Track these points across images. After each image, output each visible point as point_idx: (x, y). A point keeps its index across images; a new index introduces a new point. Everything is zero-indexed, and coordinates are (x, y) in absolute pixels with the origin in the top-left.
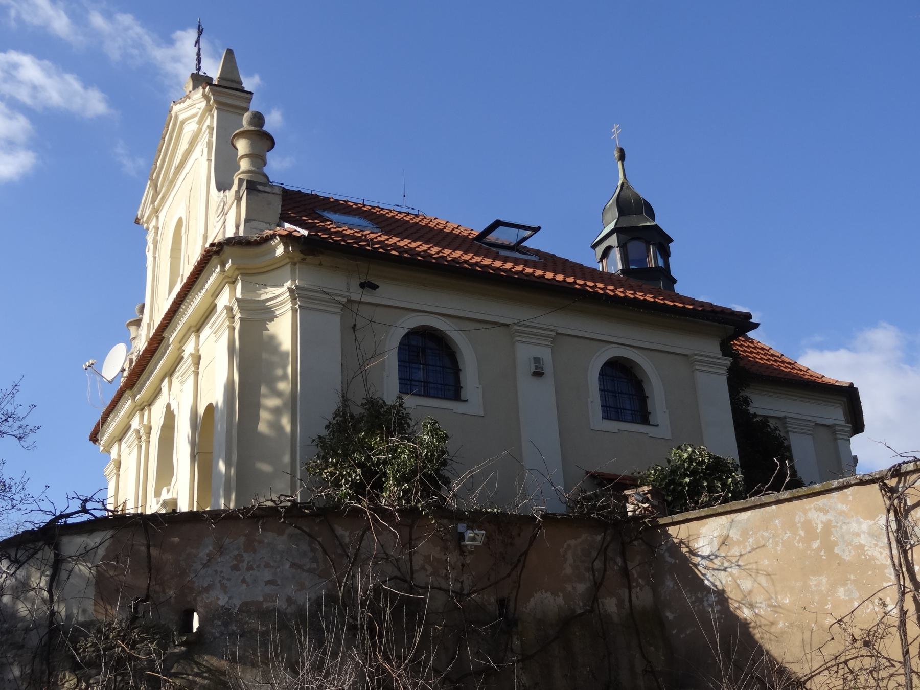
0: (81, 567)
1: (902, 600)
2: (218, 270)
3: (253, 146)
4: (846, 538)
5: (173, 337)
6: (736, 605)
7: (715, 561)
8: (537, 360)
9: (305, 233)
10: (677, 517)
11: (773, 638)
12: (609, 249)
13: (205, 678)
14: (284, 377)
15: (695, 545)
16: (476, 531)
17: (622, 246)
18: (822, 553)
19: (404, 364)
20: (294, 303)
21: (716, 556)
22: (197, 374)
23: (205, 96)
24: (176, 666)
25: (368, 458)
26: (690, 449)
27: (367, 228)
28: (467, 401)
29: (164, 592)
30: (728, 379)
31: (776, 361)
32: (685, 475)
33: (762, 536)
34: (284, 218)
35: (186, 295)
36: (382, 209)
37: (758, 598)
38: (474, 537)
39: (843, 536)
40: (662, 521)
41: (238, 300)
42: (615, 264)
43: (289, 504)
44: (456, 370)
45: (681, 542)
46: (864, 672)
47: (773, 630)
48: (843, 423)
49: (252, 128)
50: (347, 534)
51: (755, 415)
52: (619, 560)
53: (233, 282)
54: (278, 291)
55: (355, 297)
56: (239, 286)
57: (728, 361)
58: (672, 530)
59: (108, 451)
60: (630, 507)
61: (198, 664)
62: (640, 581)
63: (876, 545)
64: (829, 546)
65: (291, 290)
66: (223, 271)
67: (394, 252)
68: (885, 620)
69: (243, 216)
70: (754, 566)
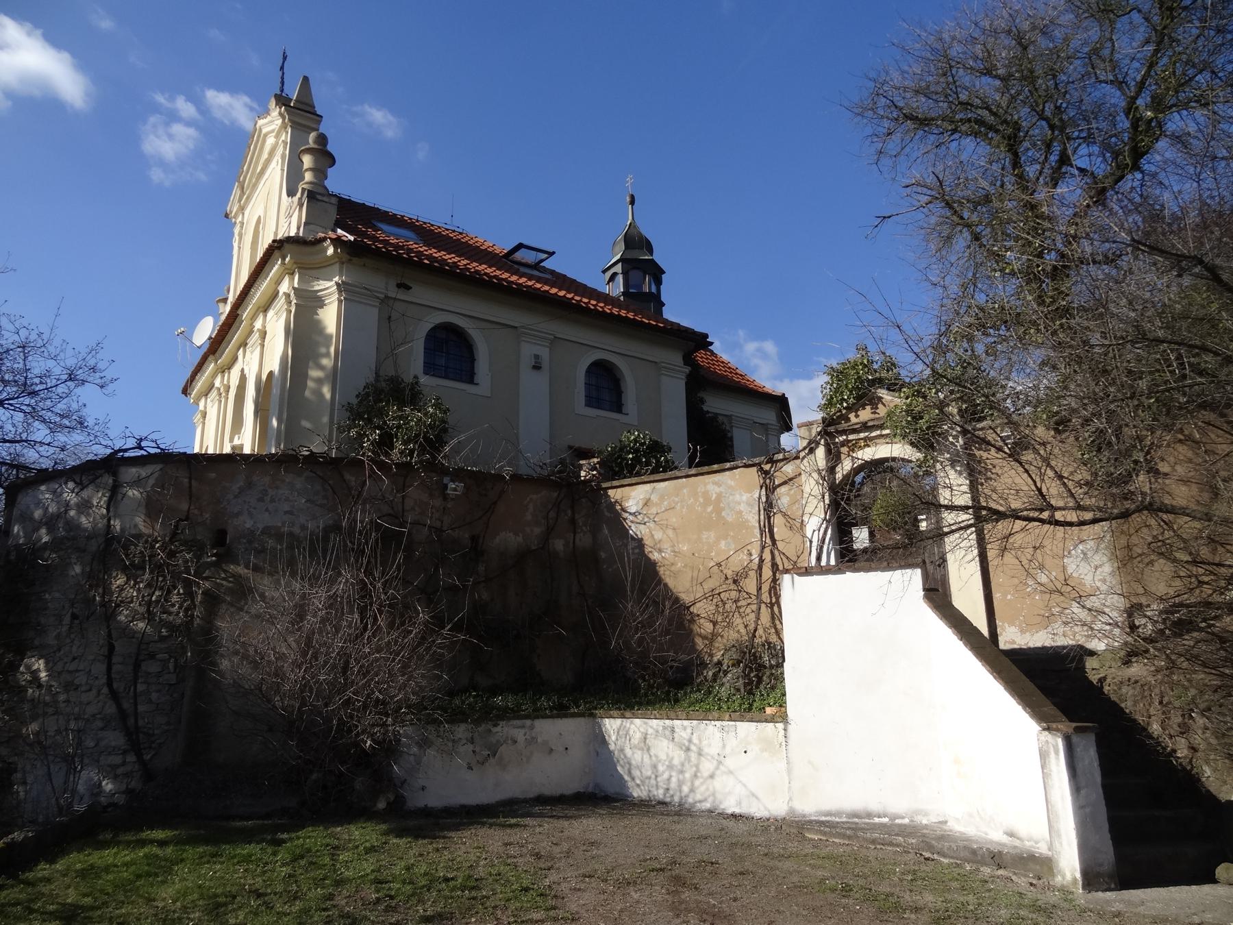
0: (135, 492)
1: (762, 552)
2: (279, 262)
3: (316, 161)
4: (731, 505)
5: (246, 315)
6: (650, 549)
7: (639, 517)
9: (352, 238)
10: (615, 483)
11: (672, 574)
12: (615, 275)
13: (230, 582)
14: (328, 355)
16: (457, 483)
17: (625, 273)
18: (714, 515)
19: (428, 350)
20: (340, 295)
21: (640, 514)
22: (263, 346)
23: (280, 114)
24: (207, 571)
25: (385, 422)
26: (636, 433)
27: (412, 239)
29: (201, 515)
31: (731, 373)
32: (630, 452)
33: (673, 500)
34: (339, 224)
35: (255, 281)
36: (432, 225)
37: (666, 546)
38: (454, 487)
39: (729, 504)
40: (604, 485)
41: (294, 288)
42: (617, 289)
43: (307, 453)
44: (472, 360)
45: (616, 502)
46: (730, 601)
47: (673, 568)
49: (316, 146)
50: (353, 479)
51: (708, 412)
52: (569, 512)
53: (292, 274)
54: (328, 284)
57: (687, 370)
58: (611, 492)
59: (197, 403)
60: (583, 473)
61: (225, 571)
62: (584, 528)
63: (750, 512)
64: (718, 511)
65: (337, 284)
66: (283, 263)
67: (426, 261)
68: (749, 566)
69: (304, 220)
70: (665, 522)
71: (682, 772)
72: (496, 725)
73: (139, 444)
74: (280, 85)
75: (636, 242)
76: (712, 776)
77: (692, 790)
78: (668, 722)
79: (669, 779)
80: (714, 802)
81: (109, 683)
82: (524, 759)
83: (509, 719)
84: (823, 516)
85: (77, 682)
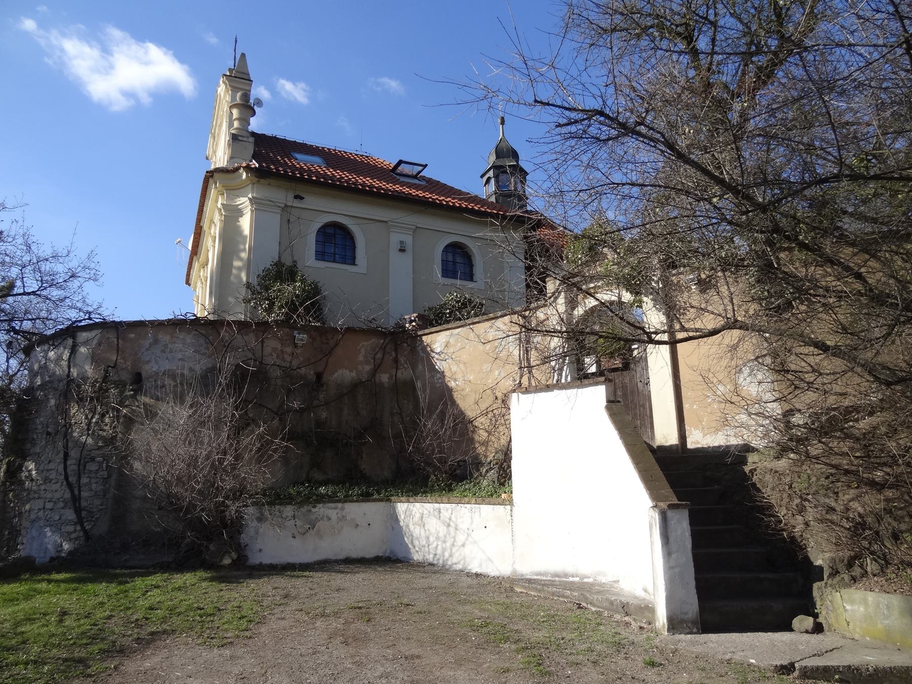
3: (240, 113)
8: (402, 242)
10: (426, 331)
14: (244, 250)
15: (434, 347)
17: (496, 177)
20: (252, 207)
37: (459, 376)
40: (420, 333)
45: (428, 345)
54: (243, 200)
55: (289, 204)
58: (424, 338)
65: (250, 199)
66: (216, 187)
67: (322, 180)
71: (445, 542)
72: (314, 507)
75: (505, 152)
76: (463, 545)
77: (451, 556)
78: (436, 505)
79: (436, 547)
80: (464, 564)
81: (66, 478)
82: (336, 532)
83: (324, 503)
85: (51, 477)
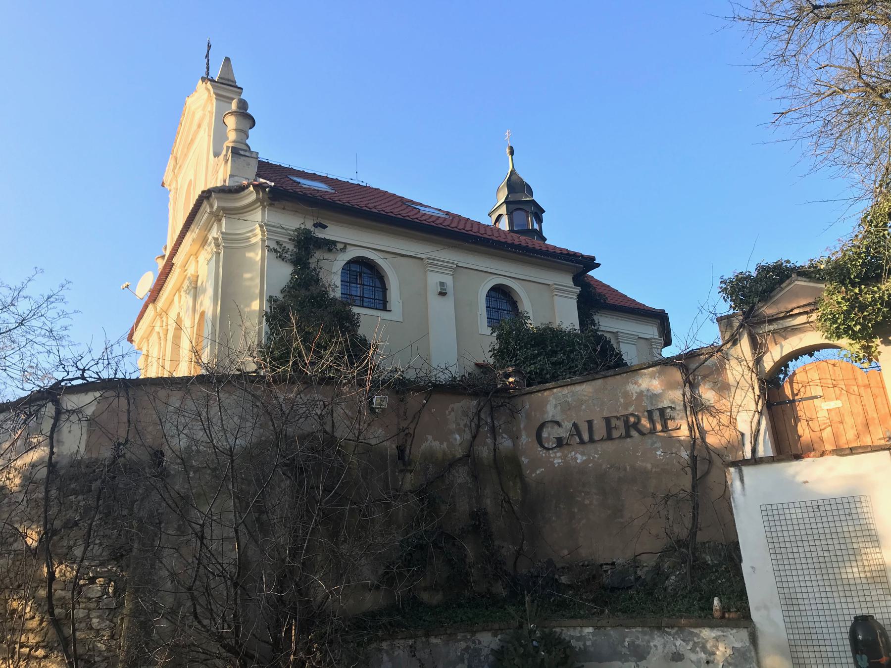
8: (442, 284)
12: (500, 216)
17: (509, 213)
28: (390, 311)
30: (577, 302)
41: (222, 233)
42: (504, 225)
44: (384, 289)
48: (657, 337)
49: (238, 110)
56: (224, 221)
57: (578, 290)
73: (83, 375)
74: (206, 70)
84: (753, 407)
